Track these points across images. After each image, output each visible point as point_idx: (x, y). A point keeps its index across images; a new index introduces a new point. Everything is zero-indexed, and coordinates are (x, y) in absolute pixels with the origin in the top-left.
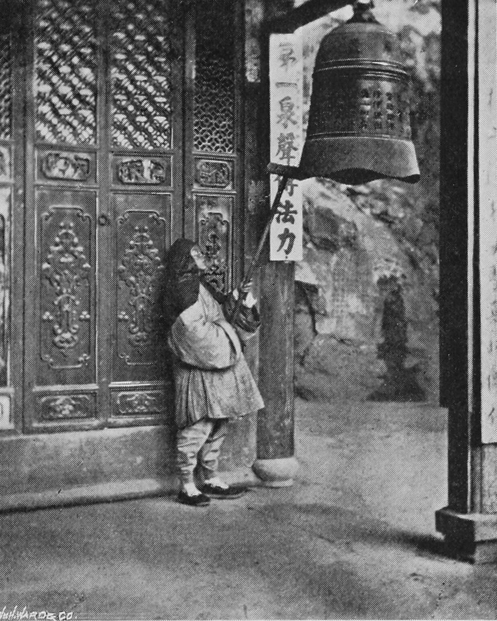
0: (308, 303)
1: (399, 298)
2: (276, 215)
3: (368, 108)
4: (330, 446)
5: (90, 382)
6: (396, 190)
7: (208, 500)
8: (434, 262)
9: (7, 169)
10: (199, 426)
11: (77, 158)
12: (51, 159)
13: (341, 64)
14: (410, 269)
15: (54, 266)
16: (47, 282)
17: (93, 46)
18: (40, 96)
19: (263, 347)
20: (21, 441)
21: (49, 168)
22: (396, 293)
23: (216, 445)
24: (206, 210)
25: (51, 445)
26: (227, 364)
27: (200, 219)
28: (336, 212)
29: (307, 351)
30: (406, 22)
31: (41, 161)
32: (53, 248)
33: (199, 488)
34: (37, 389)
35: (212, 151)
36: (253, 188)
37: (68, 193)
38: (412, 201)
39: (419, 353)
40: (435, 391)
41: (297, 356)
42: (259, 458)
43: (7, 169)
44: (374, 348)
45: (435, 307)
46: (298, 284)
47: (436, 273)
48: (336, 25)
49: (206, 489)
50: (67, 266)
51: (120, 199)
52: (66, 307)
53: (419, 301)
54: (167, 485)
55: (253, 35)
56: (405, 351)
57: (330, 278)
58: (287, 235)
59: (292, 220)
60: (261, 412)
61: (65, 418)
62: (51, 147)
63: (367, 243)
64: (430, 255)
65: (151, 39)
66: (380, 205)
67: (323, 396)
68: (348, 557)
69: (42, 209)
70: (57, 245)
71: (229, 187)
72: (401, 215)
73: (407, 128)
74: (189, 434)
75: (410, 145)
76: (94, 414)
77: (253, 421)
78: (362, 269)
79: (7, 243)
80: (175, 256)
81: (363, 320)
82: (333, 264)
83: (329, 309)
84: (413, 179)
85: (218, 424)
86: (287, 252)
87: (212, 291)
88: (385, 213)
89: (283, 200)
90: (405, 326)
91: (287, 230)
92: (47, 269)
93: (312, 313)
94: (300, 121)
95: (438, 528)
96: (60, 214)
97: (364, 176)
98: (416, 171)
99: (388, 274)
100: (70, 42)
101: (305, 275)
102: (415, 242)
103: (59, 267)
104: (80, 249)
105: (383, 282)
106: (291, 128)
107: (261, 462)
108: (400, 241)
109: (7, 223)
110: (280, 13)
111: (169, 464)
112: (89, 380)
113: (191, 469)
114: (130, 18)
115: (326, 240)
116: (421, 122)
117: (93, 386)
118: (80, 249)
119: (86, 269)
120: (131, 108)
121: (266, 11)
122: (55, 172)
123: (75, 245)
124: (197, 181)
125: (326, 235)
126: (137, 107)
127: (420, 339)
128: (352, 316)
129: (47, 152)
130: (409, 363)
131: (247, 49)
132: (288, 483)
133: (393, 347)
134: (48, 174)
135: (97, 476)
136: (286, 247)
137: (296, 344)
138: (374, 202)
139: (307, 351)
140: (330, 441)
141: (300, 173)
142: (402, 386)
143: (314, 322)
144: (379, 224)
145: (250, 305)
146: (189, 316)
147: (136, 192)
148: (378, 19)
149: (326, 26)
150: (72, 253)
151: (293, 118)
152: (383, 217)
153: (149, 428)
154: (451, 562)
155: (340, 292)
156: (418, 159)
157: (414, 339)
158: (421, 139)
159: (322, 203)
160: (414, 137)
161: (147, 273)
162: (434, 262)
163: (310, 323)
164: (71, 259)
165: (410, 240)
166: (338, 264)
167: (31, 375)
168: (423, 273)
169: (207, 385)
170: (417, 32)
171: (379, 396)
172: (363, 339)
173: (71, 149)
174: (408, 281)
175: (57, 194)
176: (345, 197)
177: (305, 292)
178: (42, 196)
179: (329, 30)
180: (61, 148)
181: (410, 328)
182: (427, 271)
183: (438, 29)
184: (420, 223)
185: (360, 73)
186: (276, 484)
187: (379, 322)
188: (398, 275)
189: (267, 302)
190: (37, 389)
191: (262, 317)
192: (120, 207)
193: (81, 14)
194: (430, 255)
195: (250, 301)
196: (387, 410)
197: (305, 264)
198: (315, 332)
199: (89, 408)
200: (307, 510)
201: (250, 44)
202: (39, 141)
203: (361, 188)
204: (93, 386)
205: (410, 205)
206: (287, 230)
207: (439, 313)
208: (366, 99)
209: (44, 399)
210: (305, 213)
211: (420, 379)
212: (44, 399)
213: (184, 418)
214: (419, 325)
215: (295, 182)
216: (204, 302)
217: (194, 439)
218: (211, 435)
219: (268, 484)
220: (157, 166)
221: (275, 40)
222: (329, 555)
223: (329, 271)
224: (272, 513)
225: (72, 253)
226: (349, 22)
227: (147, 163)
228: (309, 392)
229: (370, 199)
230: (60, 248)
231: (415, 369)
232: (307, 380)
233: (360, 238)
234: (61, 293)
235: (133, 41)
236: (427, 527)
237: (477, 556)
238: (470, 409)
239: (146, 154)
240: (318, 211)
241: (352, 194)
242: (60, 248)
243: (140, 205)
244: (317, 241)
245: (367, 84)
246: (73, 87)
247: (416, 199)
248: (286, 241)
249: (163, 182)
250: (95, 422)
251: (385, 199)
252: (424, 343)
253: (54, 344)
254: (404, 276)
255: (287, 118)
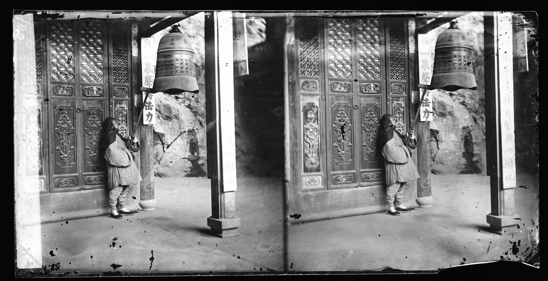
0: (435, 137)
1: (470, 135)
2: (145, 107)
3: (178, 65)
4: (446, 191)
5: (352, 170)
6: (467, 93)
7: (122, 216)
8: (483, 120)
9: (318, 89)
10: (117, 188)
11: (68, 87)
12: (335, 84)
13: (446, 45)
14: (474, 123)
15: (60, 129)
16: (335, 132)
17: (350, 40)
18: (330, 60)
19: (418, 155)
20: (326, 192)
21: (334, 88)
22: (469, 132)
23: (402, 192)
24: (395, 102)
25: (338, 193)
26: (405, 161)
27: (116, 109)
28: (445, 102)
29: (435, 156)
30: (470, 28)
31: (53, 88)
32: (60, 122)
33: (396, 209)
34: (332, 173)
35: (397, 80)
36: (413, 95)
37: (65, 101)
38: (474, 97)
39: (477, 155)
40: (485, 171)
41: (432, 157)
42: (418, 197)
43: (318, 89)
44: (461, 154)
45: (484, 137)
46: (431, 130)
47: (484, 124)
48: (443, 30)
49: (398, 209)
50: (65, 128)
51: (363, 99)
52: (65, 144)
53: (478, 136)
54: (106, 211)
55: (134, 39)
56: (473, 155)
57: (443, 127)
58: (150, 115)
59: (428, 106)
60: (418, 179)
61: (344, 183)
62: (336, 80)
63: (457, 113)
64: (482, 118)
65: (372, 37)
66: (462, 99)
67: (168, 176)
68: (453, 233)
69: (332, 104)
70: (338, 117)
71: (127, 97)
72: (470, 102)
73: (472, 69)
74: (113, 191)
75: (473, 75)
76: (355, 182)
77: (416, 183)
78: (456, 123)
79: (319, 117)
80: (384, 121)
81: (457, 143)
82: (444, 122)
83: (443, 139)
84: (474, 89)
85: (402, 184)
86: (150, 121)
87: (398, 133)
88: (464, 102)
89: (425, 98)
90: (198, 147)
91: (149, 113)
92: (57, 130)
93: (437, 141)
94: (430, 68)
95: (488, 222)
96: (339, 105)
97: (456, 88)
98: (475, 85)
99: (466, 125)
100: (341, 39)
101: (434, 126)
102: (476, 112)
103: (62, 129)
104: (347, 118)
105: (464, 128)
106: (427, 70)
107: (419, 198)
108: (470, 112)
109: (319, 109)
110: (422, 26)
111: (384, 200)
112: (76, 172)
113: (115, 205)
114: (364, 29)
115: (442, 113)
116: (477, 66)
117: (354, 171)
118: (70, 122)
119: (72, 130)
120: (365, 64)
121: (416, 26)
122: (337, 89)
123: (68, 121)
124: (114, 95)
125: (167, 114)
126: (367, 64)
127: (480, 150)
128: (452, 141)
129: (334, 82)
130: (475, 159)
131: (410, 40)
132: (430, 206)
133: (468, 153)
134: (334, 90)
135: (356, 205)
136: (149, 119)
137: (431, 153)
138: (460, 98)
139: (435, 156)
140: (445, 189)
141: (431, 87)
142: (471, 168)
143: (438, 144)
144: (462, 106)
145: (136, 142)
146: (112, 147)
147: (368, 96)
148: (459, 27)
149: (440, 30)
150: (67, 123)
151: (428, 66)
152: (463, 103)
153: (98, 190)
154: (493, 234)
155: (447, 133)
156: (476, 81)
157: (476, 150)
158: (477, 73)
159: (440, 99)
160: (474, 72)
161: (373, 127)
162: (483, 120)
163: (436, 145)
164: (66, 126)
165: (474, 112)
166: (172, 125)
167: (329, 167)
168: (479, 125)
169: (398, 170)
170: (475, 32)
171: (462, 173)
172: (456, 150)
173: (343, 80)
174: (474, 128)
175: (338, 97)
176: (448, 96)
177: (434, 133)
178: (332, 98)
179: (441, 32)
180: (62, 83)
181: (475, 146)
182: (481, 124)
183: (483, 31)
184: (477, 105)
185: (452, 49)
186: (148, 210)
187: (463, 144)
188: (469, 126)
189: (143, 141)
190: (332, 173)
191: (418, 143)
192: (362, 102)
193: (346, 28)
194: (482, 118)
195: (413, 137)
196: (467, 177)
197: (434, 122)
198: (438, 148)
199: (353, 179)
200: (438, 216)
201: (411, 39)
202: (330, 78)
203: (179, 96)
204: (354, 171)
205: (473, 99)
206: (149, 113)
207: (486, 140)
208: (455, 58)
209: (335, 176)
210: (433, 103)
211: (479, 165)
212: (335, 176)
213: (389, 183)
214: (478, 144)
215: (429, 91)
216: (118, 141)
217: (393, 190)
218: (400, 189)
219: (145, 209)
220: (99, 89)
221: (420, 36)
222: (446, 233)
223: (443, 125)
224: (422, 218)
225: (67, 123)
226: (448, 29)
227: (372, 85)
228: (163, 174)
229: (458, 97)
230: (62, 121)
231: (477, 161)
232: (437, 167)
233: (455, 112)
234: (63, 139)
235: (365, 38)
236: (204, 225)
237: (503, 232)
238: (499, 176)
239: (372, 82)
240: (438, 102)
241: (451, 95)
242: (62, 121)
243: (371, 101)
244: (438, 113)
245: (455, 53)
246: (343, 56)
247: (475, 96)
248: (426, 113)
249: (378, 92)
250: (355, 185)
251: (464, 97)
252: (480, 151)
253: (61, 158)
254: (472, 126)
255: (147, 71)
